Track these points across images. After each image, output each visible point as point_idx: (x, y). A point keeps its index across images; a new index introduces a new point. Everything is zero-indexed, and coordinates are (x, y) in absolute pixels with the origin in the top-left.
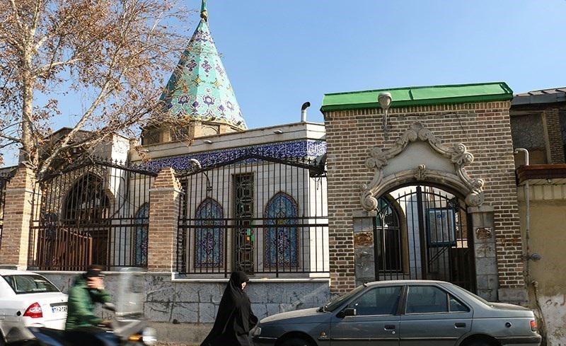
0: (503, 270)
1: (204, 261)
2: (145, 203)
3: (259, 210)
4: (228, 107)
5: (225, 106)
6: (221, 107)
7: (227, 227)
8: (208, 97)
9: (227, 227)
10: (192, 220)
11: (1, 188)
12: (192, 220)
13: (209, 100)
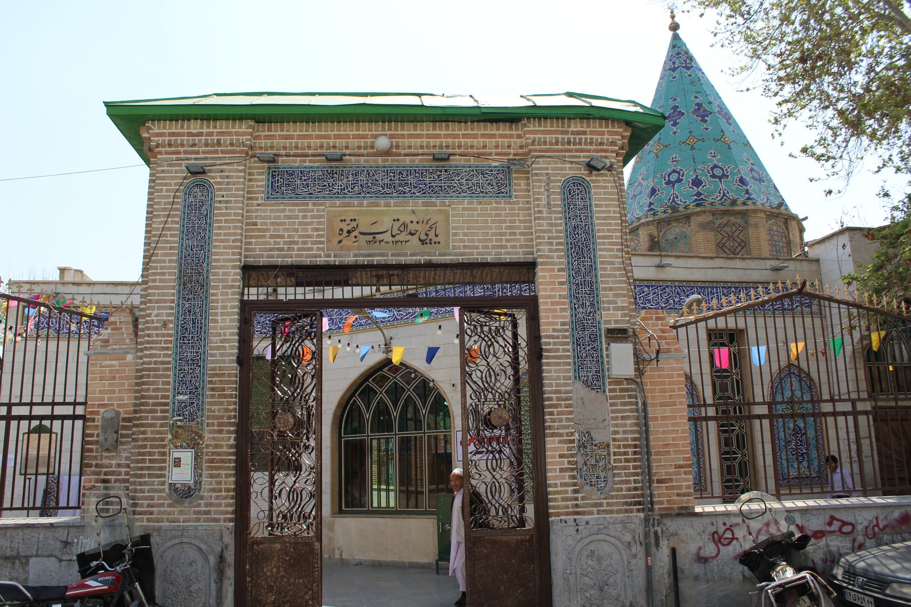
0: (635, 460)
1: (793, 473)
2: (790, 365)
3: (760, 391)
4: (753, 178)
5: (748, 179)
6: (742, 181)
7: (707, 419)
8: (716, 166)
9: (707, 419)
10: (710, 405)
11: (905, 224)
12: (710, 405)
13: (717, 172)
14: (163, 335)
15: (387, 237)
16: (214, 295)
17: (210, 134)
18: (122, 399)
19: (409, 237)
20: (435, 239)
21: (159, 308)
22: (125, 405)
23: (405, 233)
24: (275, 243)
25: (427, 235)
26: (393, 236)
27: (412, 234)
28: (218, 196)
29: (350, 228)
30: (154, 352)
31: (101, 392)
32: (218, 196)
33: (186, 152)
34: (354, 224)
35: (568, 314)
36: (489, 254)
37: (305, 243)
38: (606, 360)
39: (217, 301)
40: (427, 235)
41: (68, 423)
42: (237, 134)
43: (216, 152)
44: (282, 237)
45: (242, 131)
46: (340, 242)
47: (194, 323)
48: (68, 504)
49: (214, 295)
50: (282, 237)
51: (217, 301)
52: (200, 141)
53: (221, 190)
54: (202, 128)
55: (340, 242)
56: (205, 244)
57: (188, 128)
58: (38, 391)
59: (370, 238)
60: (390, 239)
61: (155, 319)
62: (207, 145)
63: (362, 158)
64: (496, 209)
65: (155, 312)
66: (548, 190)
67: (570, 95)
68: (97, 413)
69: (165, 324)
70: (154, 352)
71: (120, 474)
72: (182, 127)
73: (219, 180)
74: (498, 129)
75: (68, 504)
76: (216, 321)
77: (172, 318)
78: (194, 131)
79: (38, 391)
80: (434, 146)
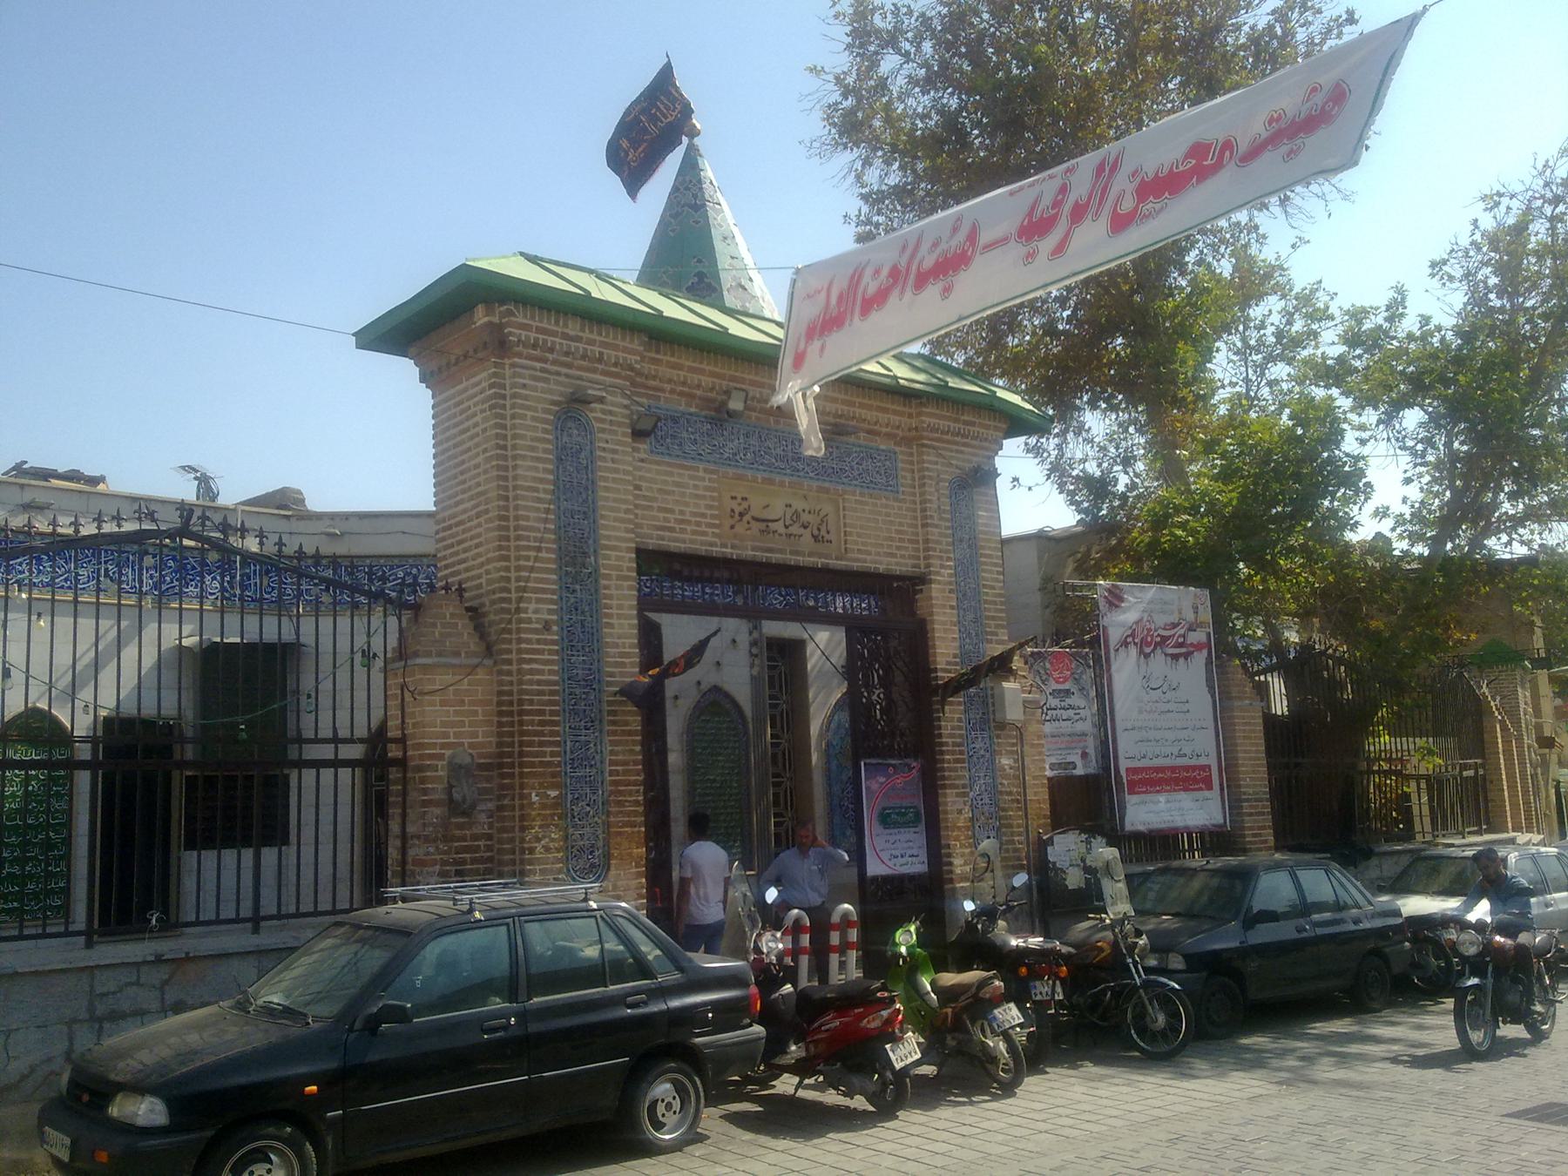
14: (546, 642)
15: (779, 527)
16: (606, 587)
17: (591, 342)
18: (475, 735)
19: (802, 531)
20: (827, 537)
21: (538, 601)
22: (482, 745)
23: (796, 525)
24: (666, 519)
25: (819, 529)
26: (786, 527)
27: (805, 527)
28: (601, 440)
29: (741, 509)
30: (535, 666)
31: (444, 724)
32: (601, 440)
33: (554, 362)
34: (745, 505)
35: (957, 644)
36: (881, 563)
37: (698, 524)
38: (990, 701)
39: (610, 597)
40: (819, 529)
41: (327, 774)
42: (625, 350)
43: (594, 371)
44: (671, 511)
45: (630, 350)
46: (732, 527)
47: (583, 626)
48: (238, 914)
49: (606, 587)
50: (671, 511)
51: (610, 597)
52: (577, 348)
53: (603, 431)
54: (582, 330)
55: (732, 527)
56: (589, 512)
57: (566, 326)
58: (343, 716)
59: (763, 526)
60: (782, 530)
61: (534, 616)
62: (584, 357)
63: (754, 414)
64: (886, 506)
65: (532, 606)
66: (937, 491)
67: (533, 260)
68: (441, 757)
69: (547, 627)
70: (535, 666)
71: (477, 849)
72: (557, 323)
73: (600, 415)
74: (893, 403)
75: (238, 914)
76: (611, 626)
77: (555, 617)
78: (572, 333)
79: (343, 716)
80: (854, 418)
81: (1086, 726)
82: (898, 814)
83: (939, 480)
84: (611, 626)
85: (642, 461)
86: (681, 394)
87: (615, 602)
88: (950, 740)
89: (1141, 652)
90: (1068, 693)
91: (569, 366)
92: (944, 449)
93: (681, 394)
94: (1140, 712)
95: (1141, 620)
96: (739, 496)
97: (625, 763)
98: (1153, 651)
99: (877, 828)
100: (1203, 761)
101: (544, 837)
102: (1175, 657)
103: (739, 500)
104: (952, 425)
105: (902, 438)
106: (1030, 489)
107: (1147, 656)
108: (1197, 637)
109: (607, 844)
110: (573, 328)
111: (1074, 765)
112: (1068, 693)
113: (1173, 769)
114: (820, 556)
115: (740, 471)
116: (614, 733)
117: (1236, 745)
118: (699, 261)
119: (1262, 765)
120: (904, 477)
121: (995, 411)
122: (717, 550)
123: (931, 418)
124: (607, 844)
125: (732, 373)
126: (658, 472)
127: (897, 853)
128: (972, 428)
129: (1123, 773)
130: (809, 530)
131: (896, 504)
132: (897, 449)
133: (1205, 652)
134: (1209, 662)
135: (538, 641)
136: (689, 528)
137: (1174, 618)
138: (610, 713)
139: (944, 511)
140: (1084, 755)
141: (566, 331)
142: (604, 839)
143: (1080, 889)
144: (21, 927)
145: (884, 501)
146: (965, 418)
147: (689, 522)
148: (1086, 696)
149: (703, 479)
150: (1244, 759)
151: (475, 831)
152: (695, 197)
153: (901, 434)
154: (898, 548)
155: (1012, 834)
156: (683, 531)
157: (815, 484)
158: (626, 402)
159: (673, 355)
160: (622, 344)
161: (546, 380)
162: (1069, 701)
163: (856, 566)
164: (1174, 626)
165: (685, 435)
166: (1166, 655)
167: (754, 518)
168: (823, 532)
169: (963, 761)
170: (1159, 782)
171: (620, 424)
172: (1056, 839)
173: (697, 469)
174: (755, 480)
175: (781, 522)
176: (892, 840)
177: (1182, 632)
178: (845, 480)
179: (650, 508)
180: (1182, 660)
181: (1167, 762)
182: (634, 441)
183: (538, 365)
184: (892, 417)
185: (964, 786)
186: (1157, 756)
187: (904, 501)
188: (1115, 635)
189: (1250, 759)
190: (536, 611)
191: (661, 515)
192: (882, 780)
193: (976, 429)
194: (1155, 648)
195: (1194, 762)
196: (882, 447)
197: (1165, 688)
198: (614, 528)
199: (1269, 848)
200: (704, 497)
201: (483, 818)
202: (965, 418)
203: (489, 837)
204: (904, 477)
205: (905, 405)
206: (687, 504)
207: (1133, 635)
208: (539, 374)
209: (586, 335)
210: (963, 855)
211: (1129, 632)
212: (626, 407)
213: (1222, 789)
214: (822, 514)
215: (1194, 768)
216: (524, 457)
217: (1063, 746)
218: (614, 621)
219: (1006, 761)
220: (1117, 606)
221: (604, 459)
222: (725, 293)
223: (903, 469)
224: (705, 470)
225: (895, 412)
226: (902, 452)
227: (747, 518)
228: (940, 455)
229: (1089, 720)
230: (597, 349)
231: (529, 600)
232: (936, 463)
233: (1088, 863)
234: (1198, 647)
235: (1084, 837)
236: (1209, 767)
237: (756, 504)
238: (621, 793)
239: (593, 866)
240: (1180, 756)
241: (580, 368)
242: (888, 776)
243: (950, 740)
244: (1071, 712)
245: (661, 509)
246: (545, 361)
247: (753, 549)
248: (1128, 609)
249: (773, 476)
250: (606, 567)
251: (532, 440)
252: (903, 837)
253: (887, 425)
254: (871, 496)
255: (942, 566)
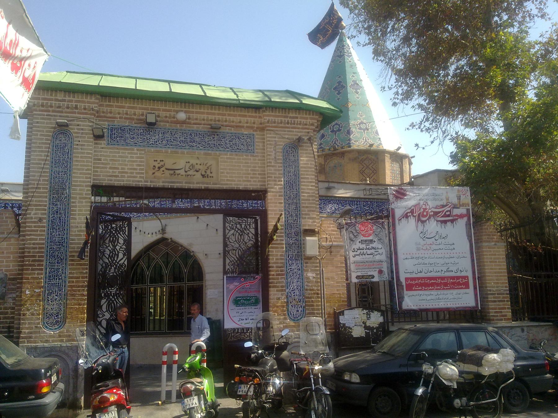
15: (182, 172)
16: (73, 203)
19: (195, 173)
20: (210, 175)
22: (10, 270)
23: (193, 170)
24: (113, 172)
25: (206, 172)
26: (186, 172)
27: (197, 171)
30: (33, 237)
33: (53, 111)
34: (162, 163)
36: (240, 185)
39: (75, 207)
40: (206, 172)
42: (88, 102)
43: (75, 113)
44: (118, 168)
45: (93, 103)
46: (154, 173)
49: (73, 203)
50: (118, 168)
51: (75, 207)
52: (63, 105)
53: (77, 137)
54: (65, 96)
59: (172, 172)
60: (184, 173)
62: (68, 108)
64: (246, 159)
66: (275, 150)
69: (40, 220)
70: (33, 237)
72: (51, 95)
74: (248, 112)
76: (75, 219)
78: (59, 98)
81: (383, 257)
82: (244, 299)
83: (276, 145)
84: (75, 219)
85: (102, 148)
86: (126, 118)
87: (78, 209)
88: (275, 265)
89: (419, 220)
90: (371, 241)
91: (62, 112)
92: (277, 131)
93: (126, 118)
94: (418, 249)
95: (419, 204)
96: (159, 160)
97: (78, 278)
98: (428, 219)
99: (232, 306)
100: (463, 274)
101: (32, 309)
102: (442, 222)
103: (159, 162)
104: (283, 119)
105: (257, 128)
106: (423, 148)
107: (423, 222)
108: (463, 211)
109: (65, 312)
110: (60, 96)
111: (373, 277)
112: (371, 241)
113: (442, 278)
114: (203, 183)
115: (158, 149)
116: (73, 265)
117: (484, 265)
118: (340, 77)
119: (504, 276)
120: (259, 146)
121: (303, 110)
122: (141, 184)
123: (268, 117)
124: (65, 312)
125: (151, 107)
126: (110, 152)
127: (244, 318)
128: (296, 120)
129: (402, 280)
130: (199, 173)
131: (252, 158)
132: (255, 133)
133: (465, 219)
134: (468, 224)
135: (35, 227)
136: (126, 175)
137: (444, 202)
138: (42, 257)
139: (278, 159)
140: (381, 272)
141: (57, 98)
142: (64, 310)
143: (361, 338)
144: (399, 319)
145: (245, 157)
146: (291, 115)
147: (127, 173)
148: (383, 243)
149: (137, 154)
150: (490, 272)
151: (5, 305)
152: (341, 52)
153: (255, 126)
154: (251, 178)
155: (313, 309)
156: (124, 177)
157: (202, 152)
158: (91, 124)
159: (142, 105)
160: (86, 100)
161: (50, 119)
162: (371, 245)
163: (225, 187)
164: (443, 206)
165: (128, 135)
166: (437, 221)
167: (167, 169)
168: (208, 172)
169: (283, 275)
170: (432, 285)
171: (86, 134)
172: (346, 312)
173: (133, 150)
174: (167, 152)
175: (183, 170)
176: (241, 311)
177: (449, 209)
178: (221, 149)
179: (106, 168)
180: (449, 224)
181: (438, 275)
182: (95, 140)
183: (46, 113)
184: (249, 119)
185: (282, 287)
186: (421, 272)
187: (256, 156)
188: (398, 213)
189: (495, 273)
190: (35, 214)
191: (111, 170)
192: (237, 284)
193: (299, 120)
194: (430, 218)
195: (458, 274)
196: (245, 133)
197: (437, 238)
198: (79, 177)
199: (508, 319)
200: (136, 161)
201: (10, 300)
202: (291, 115)
203: (13, 308)
204: (259, 146)
205: (256, 112)
206: (126, 165)
207: (412, 212)
208: (46, 117)
209: (67, 98)
210: (279, 319)
211: (409, 211)
212: (90, 126)
213: (475, 288)
214: (208, 165)
215: (458, 278)
216: (35, 151)
217: (367, 267)
218: (77, 217)
219: (310, 275)
220: (401, 198)
221: (77, 149)
222: (348, 87)
223: (257, 142)
224: (138, 150)
225: (250, 116)
226: (257, 134)
227: (162, 169)
228: (277, 134)
229: (384, 253)
230: (41, 101)
231: (32, 210)
232: (275, 137)
233: (368, 324)
234: (461, 216)
235: (365, 311)
236: (467, 277)
237: (169, 163)
238: (75, 291)
239: (57, 322)
240: (448, 271)
241: (66, 112)
242: (241, 282)
243: (275, 265)
244: (373, 251)
245: (111, 168)
246: (49, 111)
247: (163, 182)
248: (410, 199)
249: (177, 150)
250: (74, 194)
251: (39, 144)
252: (247, 311)
253: (247, 123)
254: (237, 155)
255: (275, 185)
